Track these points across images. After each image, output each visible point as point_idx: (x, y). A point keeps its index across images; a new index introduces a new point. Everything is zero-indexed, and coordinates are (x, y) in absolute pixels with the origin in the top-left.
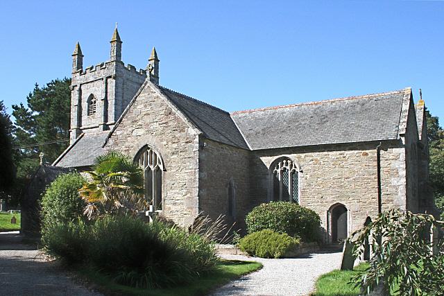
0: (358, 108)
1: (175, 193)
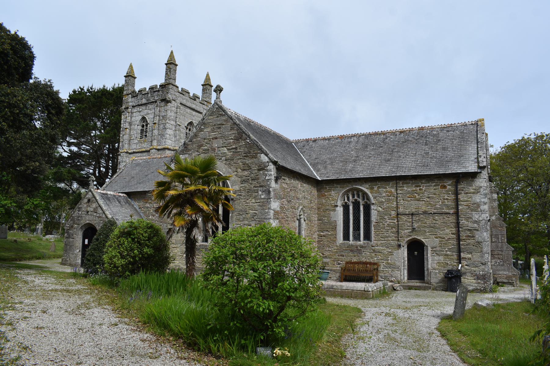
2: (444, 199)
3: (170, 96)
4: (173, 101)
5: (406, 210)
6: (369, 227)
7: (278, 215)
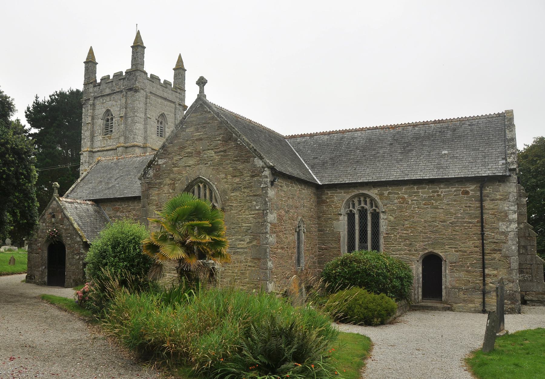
0: (449, 134)
1: (237, 239)
2: (466, 207)
3: (137, 84)
4: (142, 91)
5: (421, 219)
6: (378, 238)
7: (275, 228)
